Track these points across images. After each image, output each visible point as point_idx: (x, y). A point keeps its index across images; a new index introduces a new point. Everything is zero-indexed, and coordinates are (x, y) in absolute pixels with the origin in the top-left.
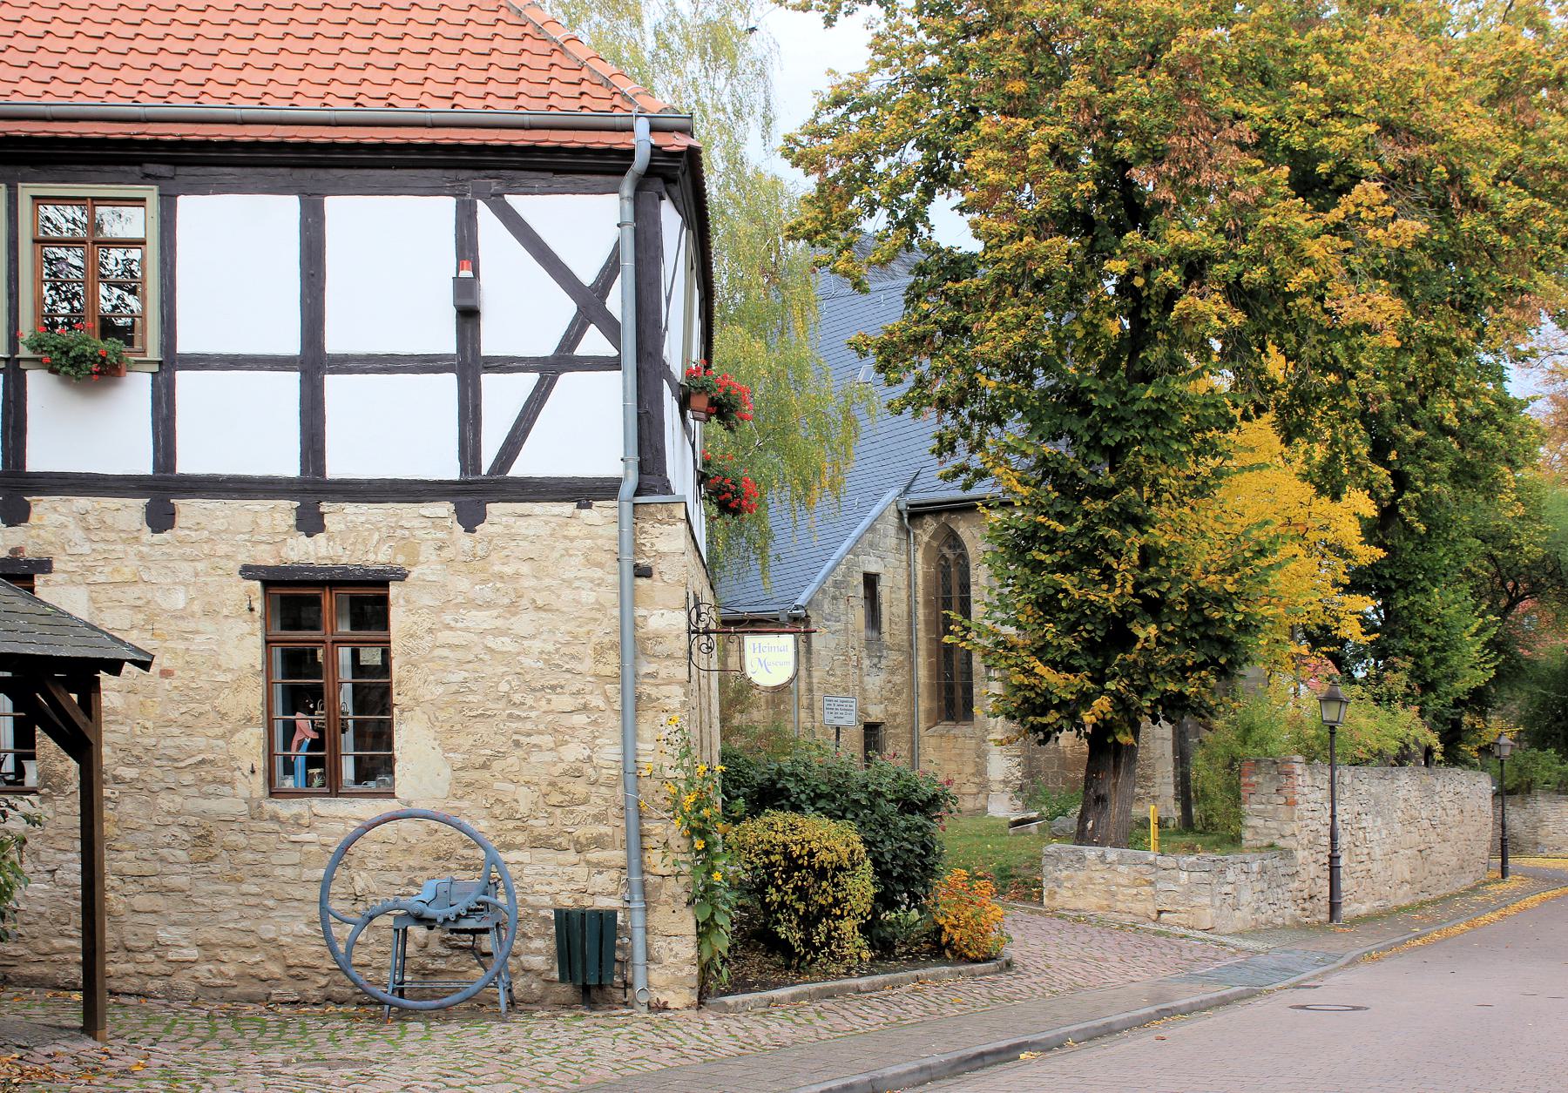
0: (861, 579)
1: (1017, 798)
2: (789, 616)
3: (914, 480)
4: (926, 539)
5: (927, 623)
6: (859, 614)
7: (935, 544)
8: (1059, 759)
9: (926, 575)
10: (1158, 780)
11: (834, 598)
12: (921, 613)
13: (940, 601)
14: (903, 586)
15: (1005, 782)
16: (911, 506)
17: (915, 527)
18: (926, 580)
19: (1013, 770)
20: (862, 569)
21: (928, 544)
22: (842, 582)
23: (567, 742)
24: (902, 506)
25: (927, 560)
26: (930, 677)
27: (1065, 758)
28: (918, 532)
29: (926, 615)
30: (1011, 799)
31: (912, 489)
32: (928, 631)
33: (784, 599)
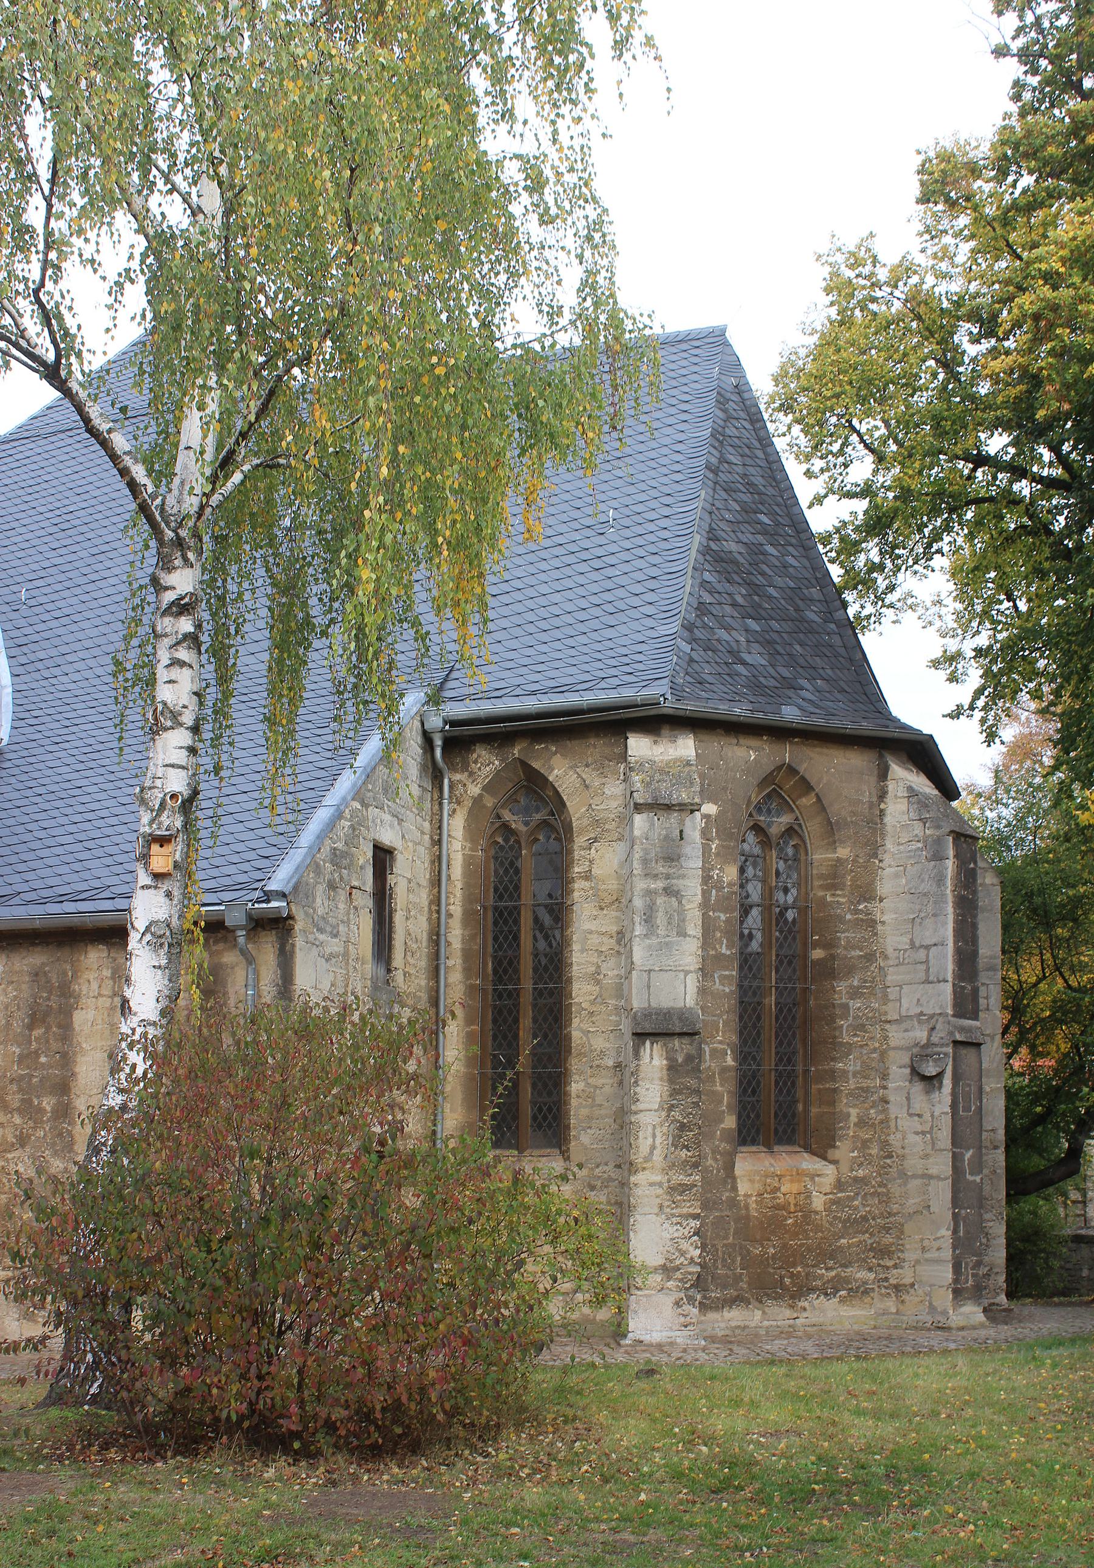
0: (370, 854)
1: (691, 1300)
2: (250, 916)
3: (446, 679)
4: (474, 790)
5: (467, 955)
6: (365, 925)
7: (489, 802)
8: (737, 1220)
9: (468, 861)
10: (911, 1255)
11: (332, 886)
12: (456, 935)
13: (490, 914)
14: (424, 882)
15: (667, 1270)
16: (454, 723)
17: (453, 768)
18: (468, 873)
19: (685, 1245)
20: (371, 836)
21: (477, 801)
22: (345, 854)
23: (165, 704)
24: (435, 722)
25: (472, 833)
26: (470, 1061)
27: (748, 1217)
28: (457, 777)
29: (465, 941)
30: (678, 1304)
31: (448, 694)
32: (467, 971)
33: (227, 881)
